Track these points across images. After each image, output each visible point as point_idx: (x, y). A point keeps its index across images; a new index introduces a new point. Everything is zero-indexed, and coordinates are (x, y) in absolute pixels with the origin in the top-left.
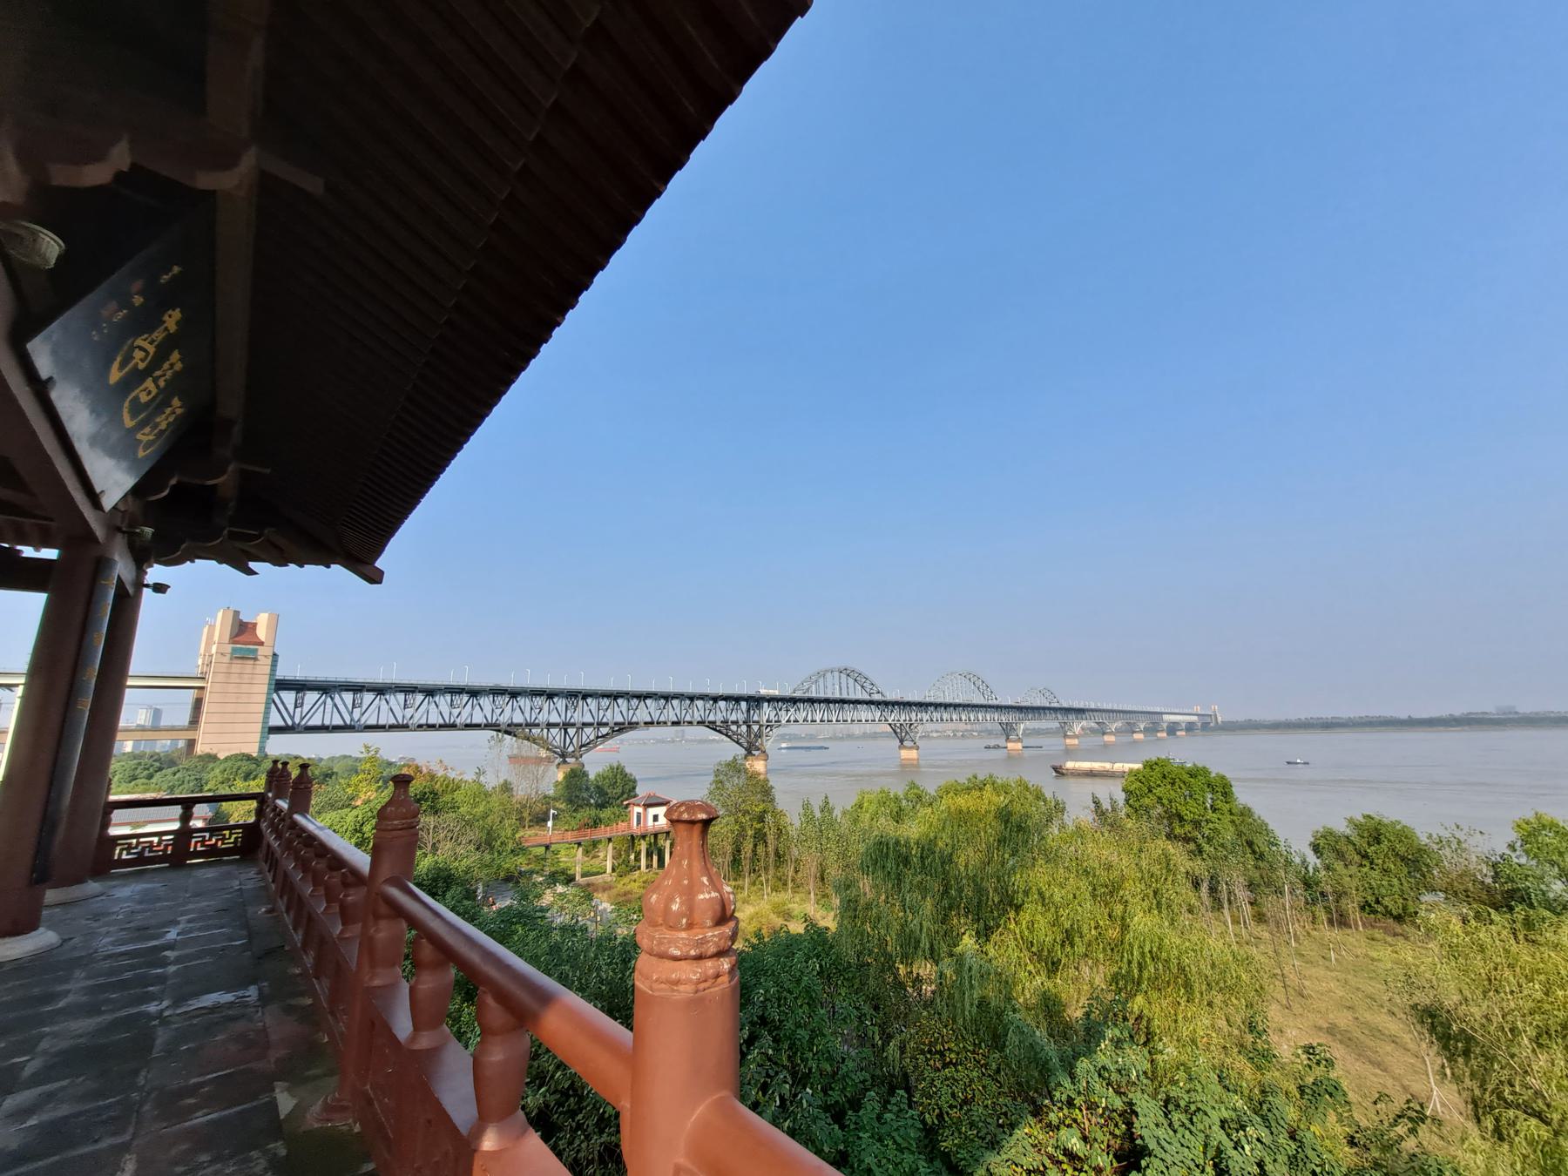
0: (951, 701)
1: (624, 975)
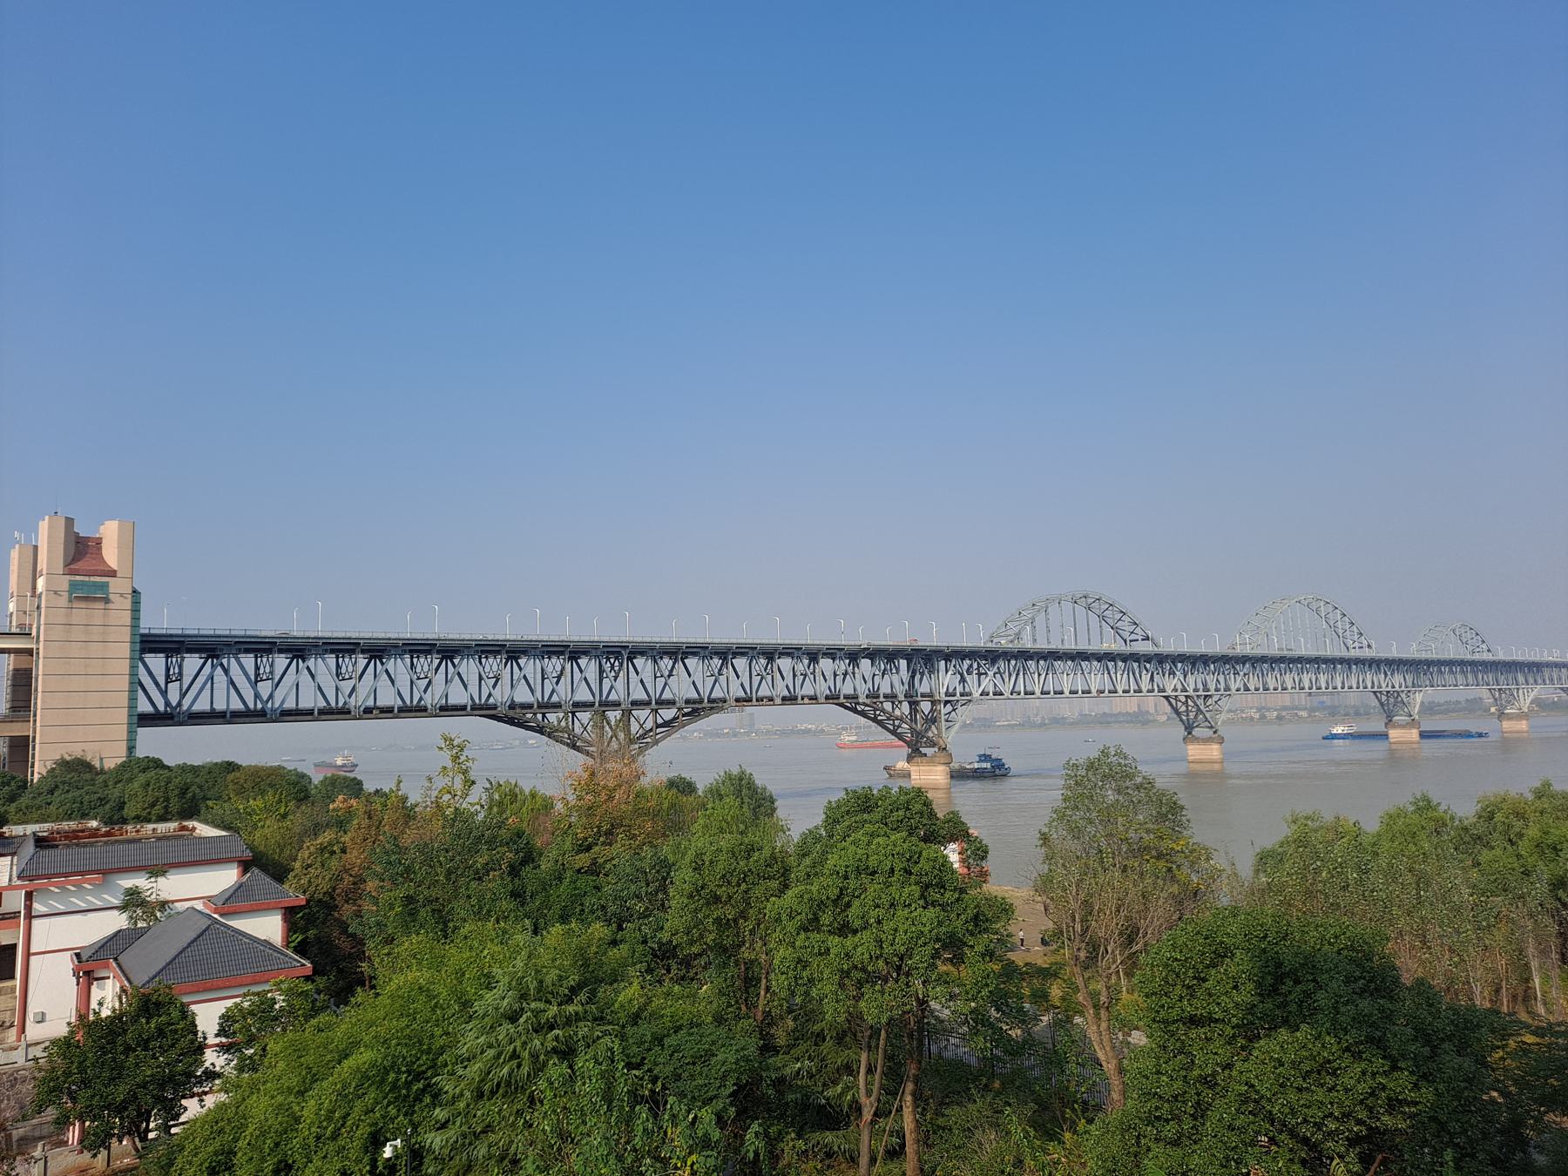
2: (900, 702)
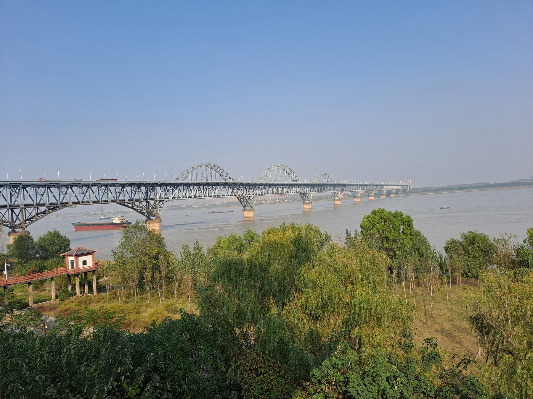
0: (273, 182)
1: (60, 358)
2: (142, 202)
